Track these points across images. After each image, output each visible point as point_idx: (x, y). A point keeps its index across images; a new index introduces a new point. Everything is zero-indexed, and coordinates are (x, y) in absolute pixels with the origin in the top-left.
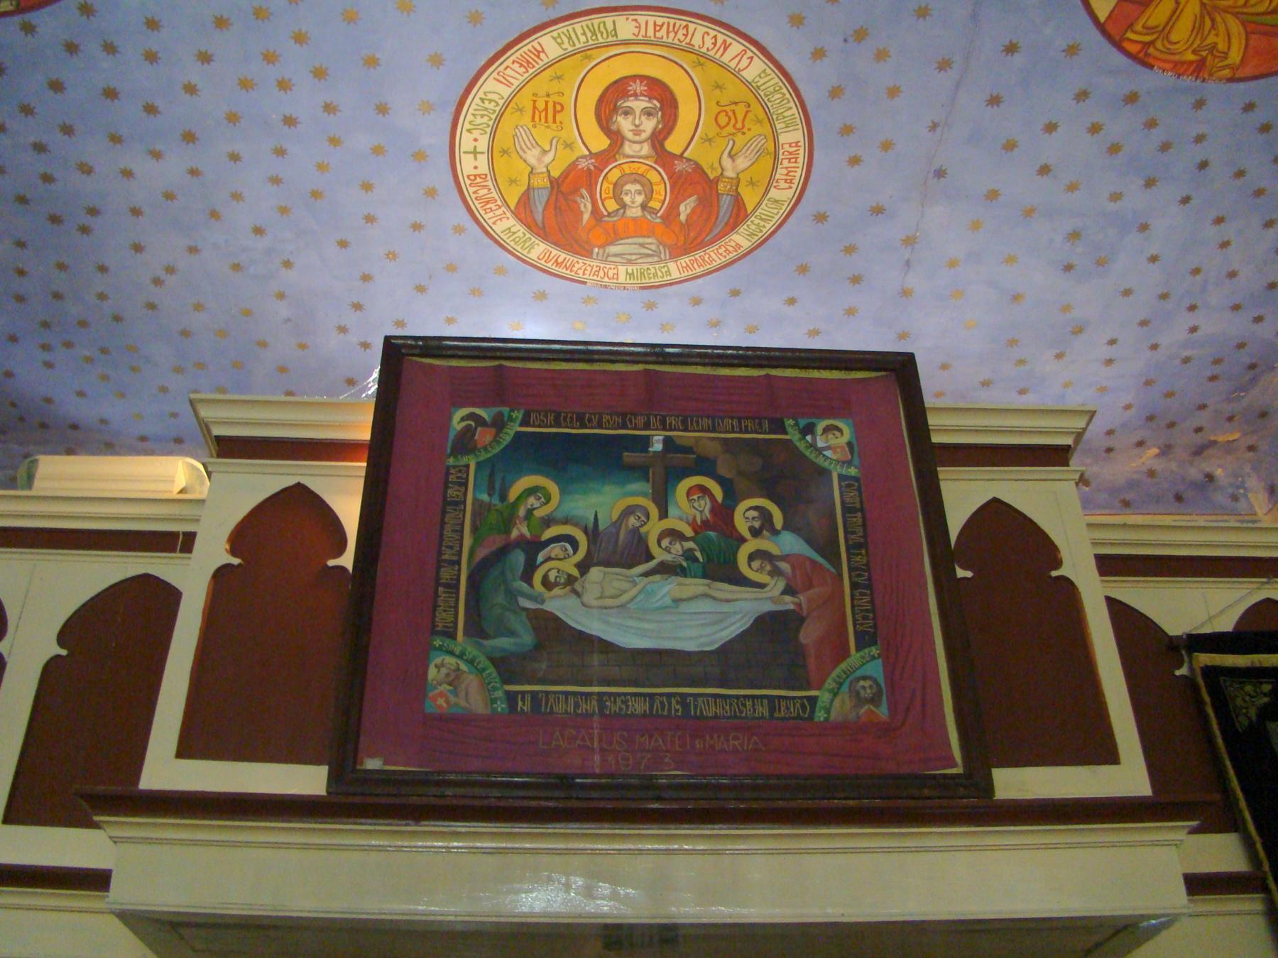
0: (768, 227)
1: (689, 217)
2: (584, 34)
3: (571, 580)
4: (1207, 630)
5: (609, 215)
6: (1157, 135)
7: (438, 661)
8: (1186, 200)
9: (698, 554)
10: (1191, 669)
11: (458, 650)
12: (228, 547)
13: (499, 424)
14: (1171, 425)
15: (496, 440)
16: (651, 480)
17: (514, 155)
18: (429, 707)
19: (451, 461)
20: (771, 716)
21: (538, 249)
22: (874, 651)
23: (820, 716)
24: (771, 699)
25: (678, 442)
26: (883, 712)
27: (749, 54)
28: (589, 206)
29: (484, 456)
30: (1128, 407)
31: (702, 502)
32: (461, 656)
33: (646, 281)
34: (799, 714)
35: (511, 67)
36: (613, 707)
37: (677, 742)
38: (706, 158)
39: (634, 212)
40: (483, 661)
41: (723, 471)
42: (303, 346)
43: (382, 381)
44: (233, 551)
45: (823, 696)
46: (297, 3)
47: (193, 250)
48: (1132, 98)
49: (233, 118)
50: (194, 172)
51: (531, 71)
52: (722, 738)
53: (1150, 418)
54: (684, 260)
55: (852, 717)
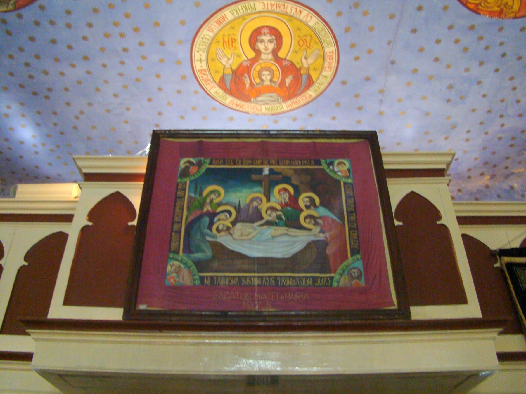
0: (323, 87)
1: (290, 84)
2: (242, 9)
3: (228, 229)
4: (508, 247)
5: (257, 84)
6: (483, 44)
7: (172, 263)
8: (497, 70)
9: (283, 217)
10: (501, 264)
11: (180, 259)
12: (88, 218)
13: (200, 164)
14: (495, 166)
15: (198, 171)
16: (263, 186)
17: (217, 61)
18: (167, 283)
19: (179, 180)
20: (314, 284)
21: (229, 100)
22: (359, 256)
23: (335, 284)
24: (313, 278)
25: (275, 170)
26: (362, 283)
27: (311, 15)
28: (249, 81)
29: (192, 178)
30: (476, 159)
31: (285, 195)
32: (181, 261)
33: (274, 112)
34: (325, 284)
35: (213, 24)
36: (244, 282)
37: (272, 296)
38: (296, 59)
39: (267, 83)
40: (190, 263)
41: (294, 182)
42: (136, 142)
43: (151, 149)
44: (90, 220)
45: (336, 276)
46: (125, 1)
47: (90, 104)
48: (472, 28)
49: (102, 50)
50: (88, 72)
51: (221, 26)
52: (292, 295)
53: (486, 163)
54: (289, 102)
55: (349, 285)
